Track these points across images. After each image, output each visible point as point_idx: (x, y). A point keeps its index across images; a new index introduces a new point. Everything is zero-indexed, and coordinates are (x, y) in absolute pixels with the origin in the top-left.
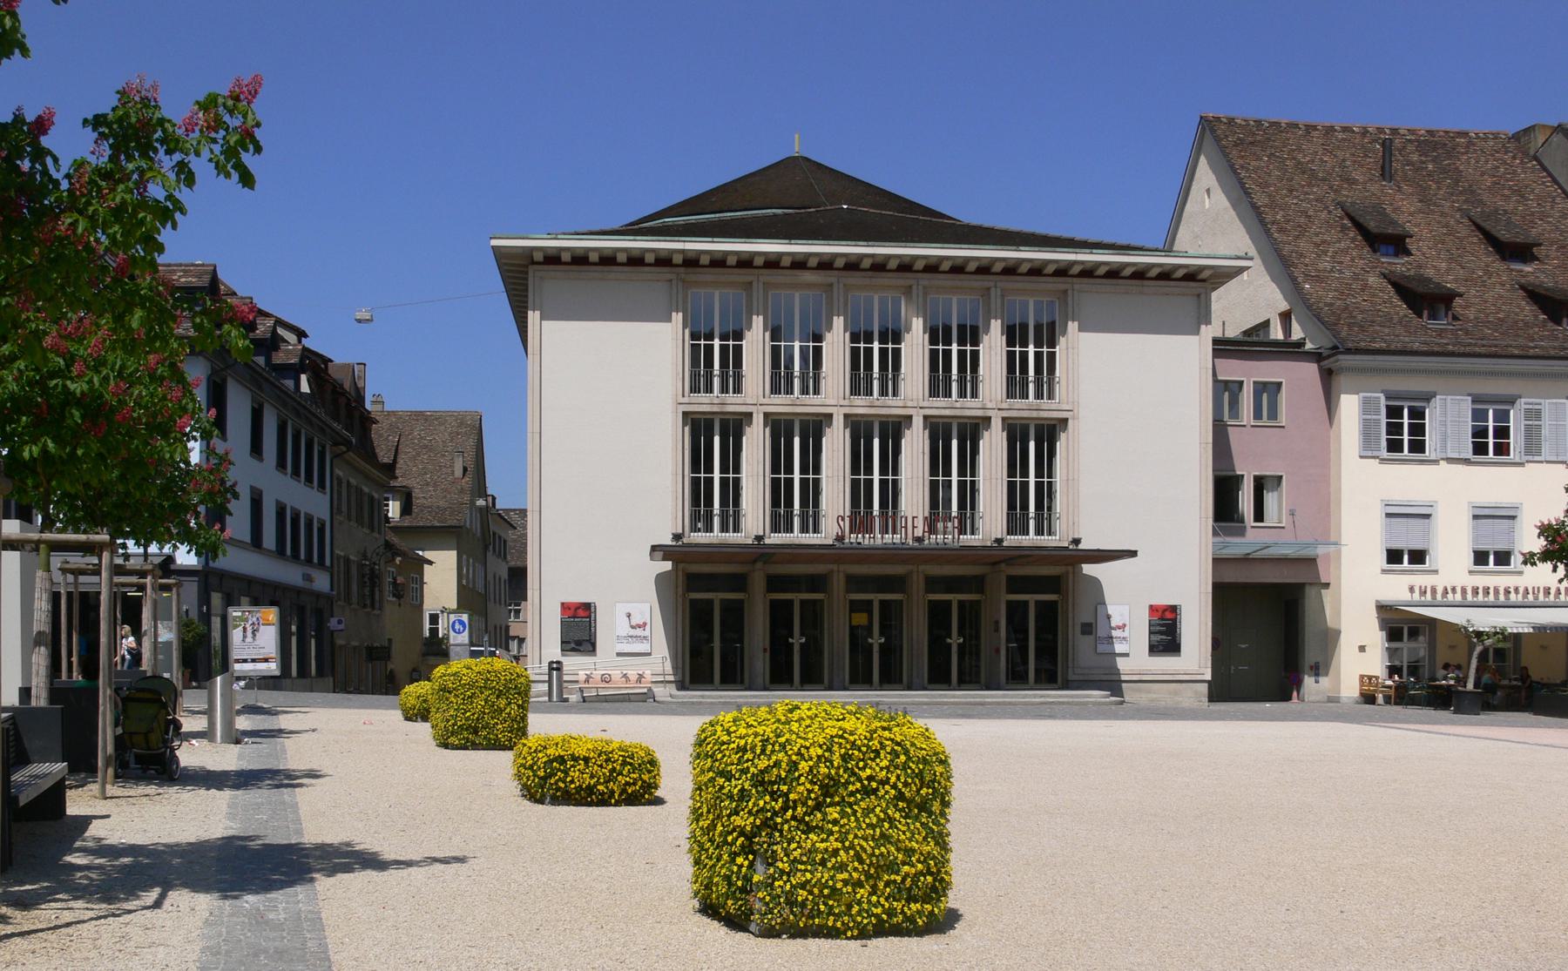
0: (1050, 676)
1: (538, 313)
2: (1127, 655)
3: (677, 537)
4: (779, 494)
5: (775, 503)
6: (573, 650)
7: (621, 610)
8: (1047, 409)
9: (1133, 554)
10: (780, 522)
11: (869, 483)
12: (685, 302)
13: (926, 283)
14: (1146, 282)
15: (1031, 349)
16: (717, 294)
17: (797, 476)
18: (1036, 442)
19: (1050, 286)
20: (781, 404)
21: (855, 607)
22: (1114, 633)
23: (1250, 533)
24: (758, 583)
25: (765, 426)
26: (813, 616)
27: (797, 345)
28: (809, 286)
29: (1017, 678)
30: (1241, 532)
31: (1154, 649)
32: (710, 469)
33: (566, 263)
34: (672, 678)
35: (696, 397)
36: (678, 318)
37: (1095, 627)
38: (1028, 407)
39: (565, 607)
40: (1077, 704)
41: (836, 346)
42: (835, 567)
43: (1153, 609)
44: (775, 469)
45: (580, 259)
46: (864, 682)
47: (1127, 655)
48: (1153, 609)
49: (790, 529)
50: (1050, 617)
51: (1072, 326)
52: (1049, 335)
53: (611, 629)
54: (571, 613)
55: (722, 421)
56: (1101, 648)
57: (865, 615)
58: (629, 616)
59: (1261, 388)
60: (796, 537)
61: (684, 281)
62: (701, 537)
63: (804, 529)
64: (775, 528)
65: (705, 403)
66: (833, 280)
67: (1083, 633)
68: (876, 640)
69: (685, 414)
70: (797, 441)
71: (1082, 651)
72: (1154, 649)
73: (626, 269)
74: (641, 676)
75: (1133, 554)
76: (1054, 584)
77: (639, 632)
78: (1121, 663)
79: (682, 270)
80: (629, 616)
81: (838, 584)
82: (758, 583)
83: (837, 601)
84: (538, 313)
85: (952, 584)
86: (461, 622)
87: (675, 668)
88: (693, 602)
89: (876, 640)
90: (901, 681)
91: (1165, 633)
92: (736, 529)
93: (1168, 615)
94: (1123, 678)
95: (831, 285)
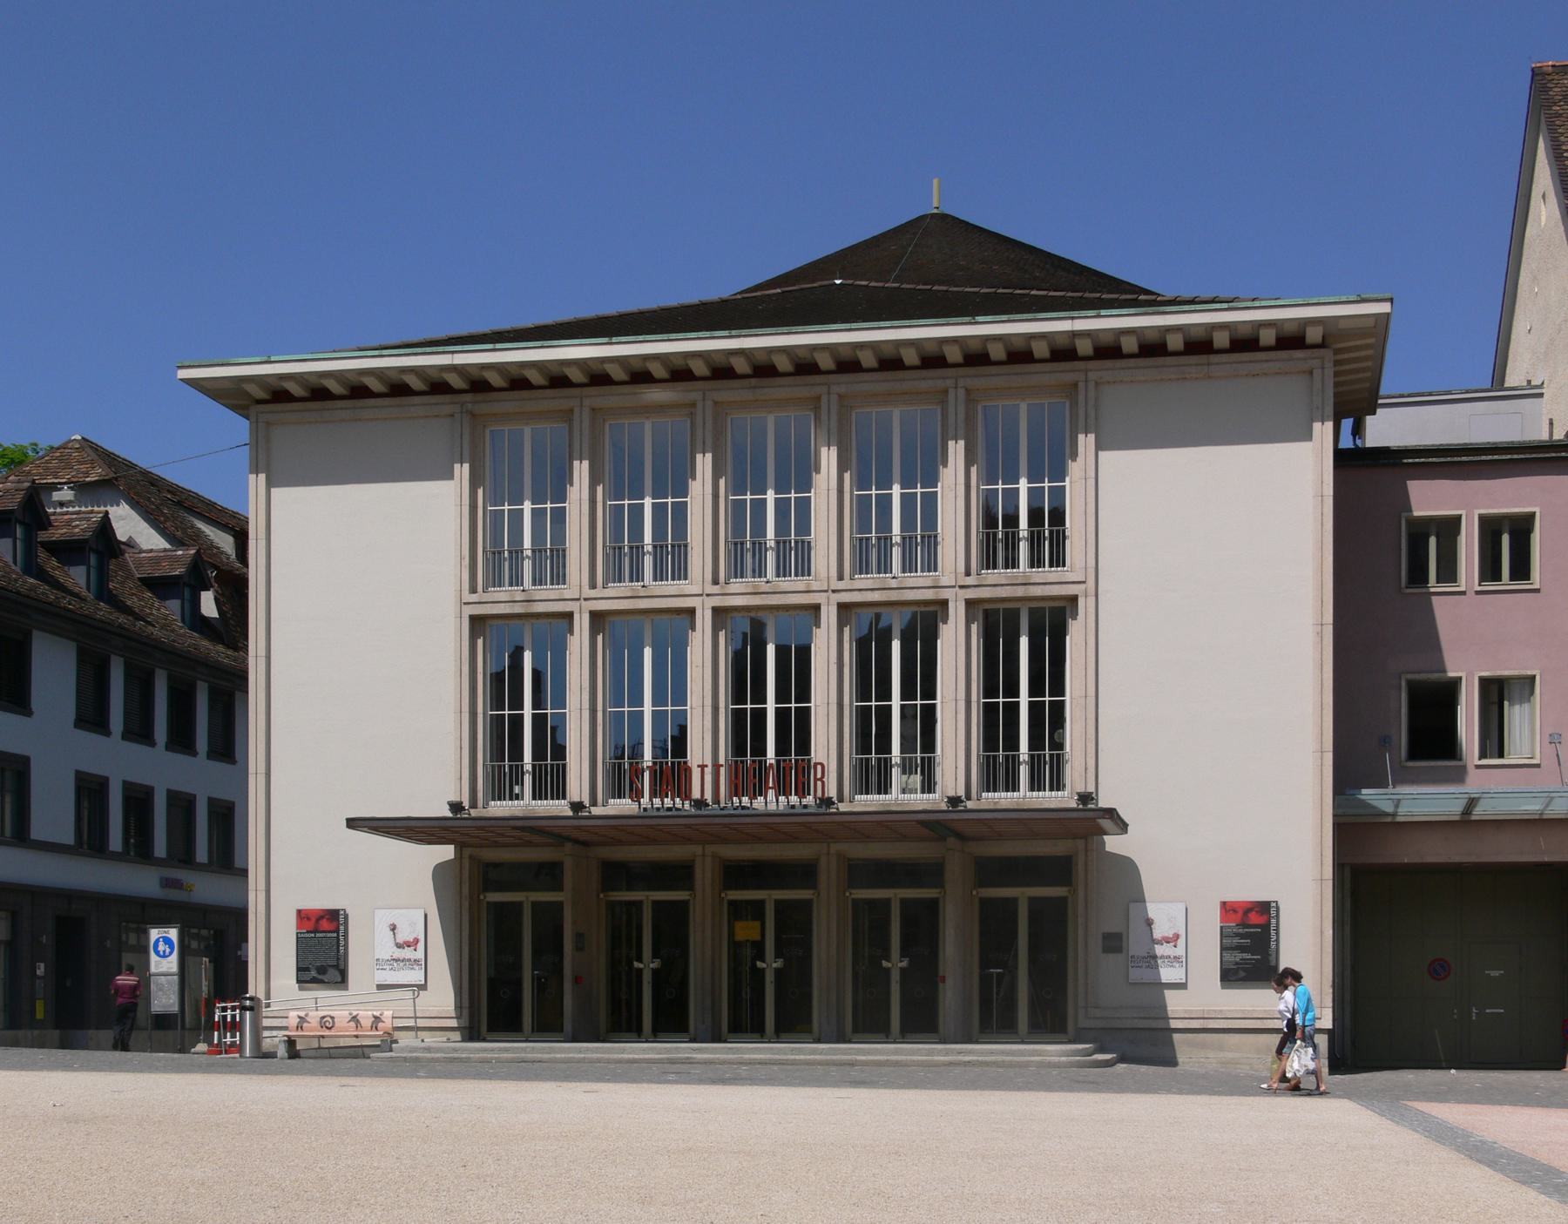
0: (1050, 1022)
1: (1091, 437)
2: (1182, 986)
3: (456, 807)
4: (996, 727)
5: (989, 742)
6: (314, 981)
7: (383, 918)
8: (1045, 582)
9: (353, 823)
10: (998, 774)
11: (1013, 709)
12: (718, 434)
13: (842, 389)
14: (1214, 358)
15: (896, 491)
16: (896, 414)
17: (1024, 699)
18: (1030, 645)
19: (924, 385)
20: (998, 583)
21: (738, 911)
22: (1160, 950)
23: (1476, 782)
24: (956, 871)
25: (969, 622)
26: (673, 923)
27: (648, 502)
28: (661, 409)
29: (868, 1023)
30: (1459, 776)
31: (1231, 976)
32: (885, 694)
33: (1176, 354)
34: (454, 1023)
35: (992, 576)
36: (463, 471)
37: (1126, 940)
38: (1025, 580)
39: (302, 916)
40: (1011, 1065)
41: (954, 489)
42: (698, 849)
43: (1227, 908)
44: (990, 689)
45: (357, 390)
46: (629, 1030)
47: (1182, 986)
48: (1227, 908)
49: (1012, 785)
50: (1052, 925)
51: (1086, 442)
52: (1052, 461)
53: (369, 948)
54: (311, 925)
55: (1032, 612)
56: (1136, 974)
57: (757, 924)
58: (393, 928)
59: (1491, 528)
60: (1024, 796)
61: (473, 415)
62: (501, 808)
63: (1036, 784)
64: (990, 784)
65: (502, 600)
66: (695, 396)
67: (1107, 950)
68: (771, 964)
69: (474, 620)
70: (1024, 642)
71: (1097, 982)
72: (1231, 976)
73: (1141, 362)
74: (377, 1019)
75: (353, 823)
76: (1061, 870)
77: (407, 953)
78: (1175, 1003)
79: (468, 397)
80: (393, 928)
81: (705, 875)
82: (956, 871)
83: (703, 902)
84: (1091, 437)
85: (886, 873)
86: (168, 941)
87: (459, 1006)
88: (985, 903)
89: (771, 964)
90: (562, 1030)
91: (1251, 948)
92: (1057, 784)
93: (1254, 918)
94: (1174, 1024)
95: (693, 405)
